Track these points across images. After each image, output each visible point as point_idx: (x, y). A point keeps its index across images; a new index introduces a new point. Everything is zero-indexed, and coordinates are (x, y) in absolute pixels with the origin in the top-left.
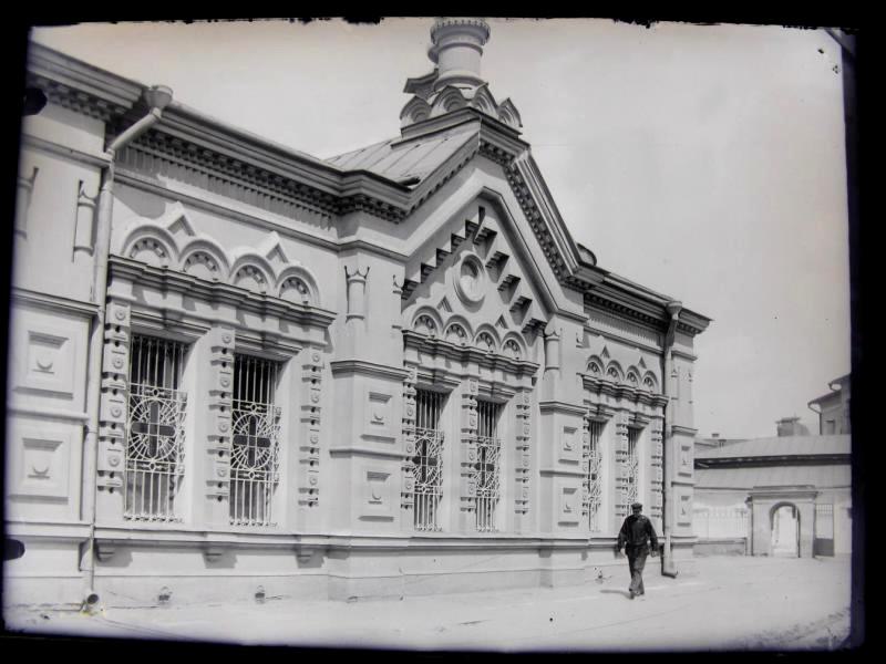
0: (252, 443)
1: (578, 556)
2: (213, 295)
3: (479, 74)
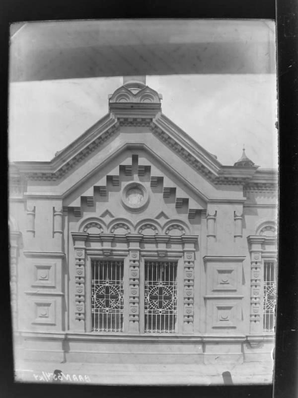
1: (200, 347)
2: (127, 240)
3: (145, 82)
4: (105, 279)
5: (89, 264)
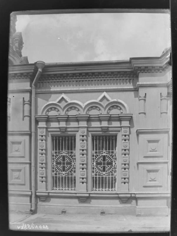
0: (64, 164)
1: (134, 201)
2: (77, 119)
4: (102, 150)
5: (90, 139)
